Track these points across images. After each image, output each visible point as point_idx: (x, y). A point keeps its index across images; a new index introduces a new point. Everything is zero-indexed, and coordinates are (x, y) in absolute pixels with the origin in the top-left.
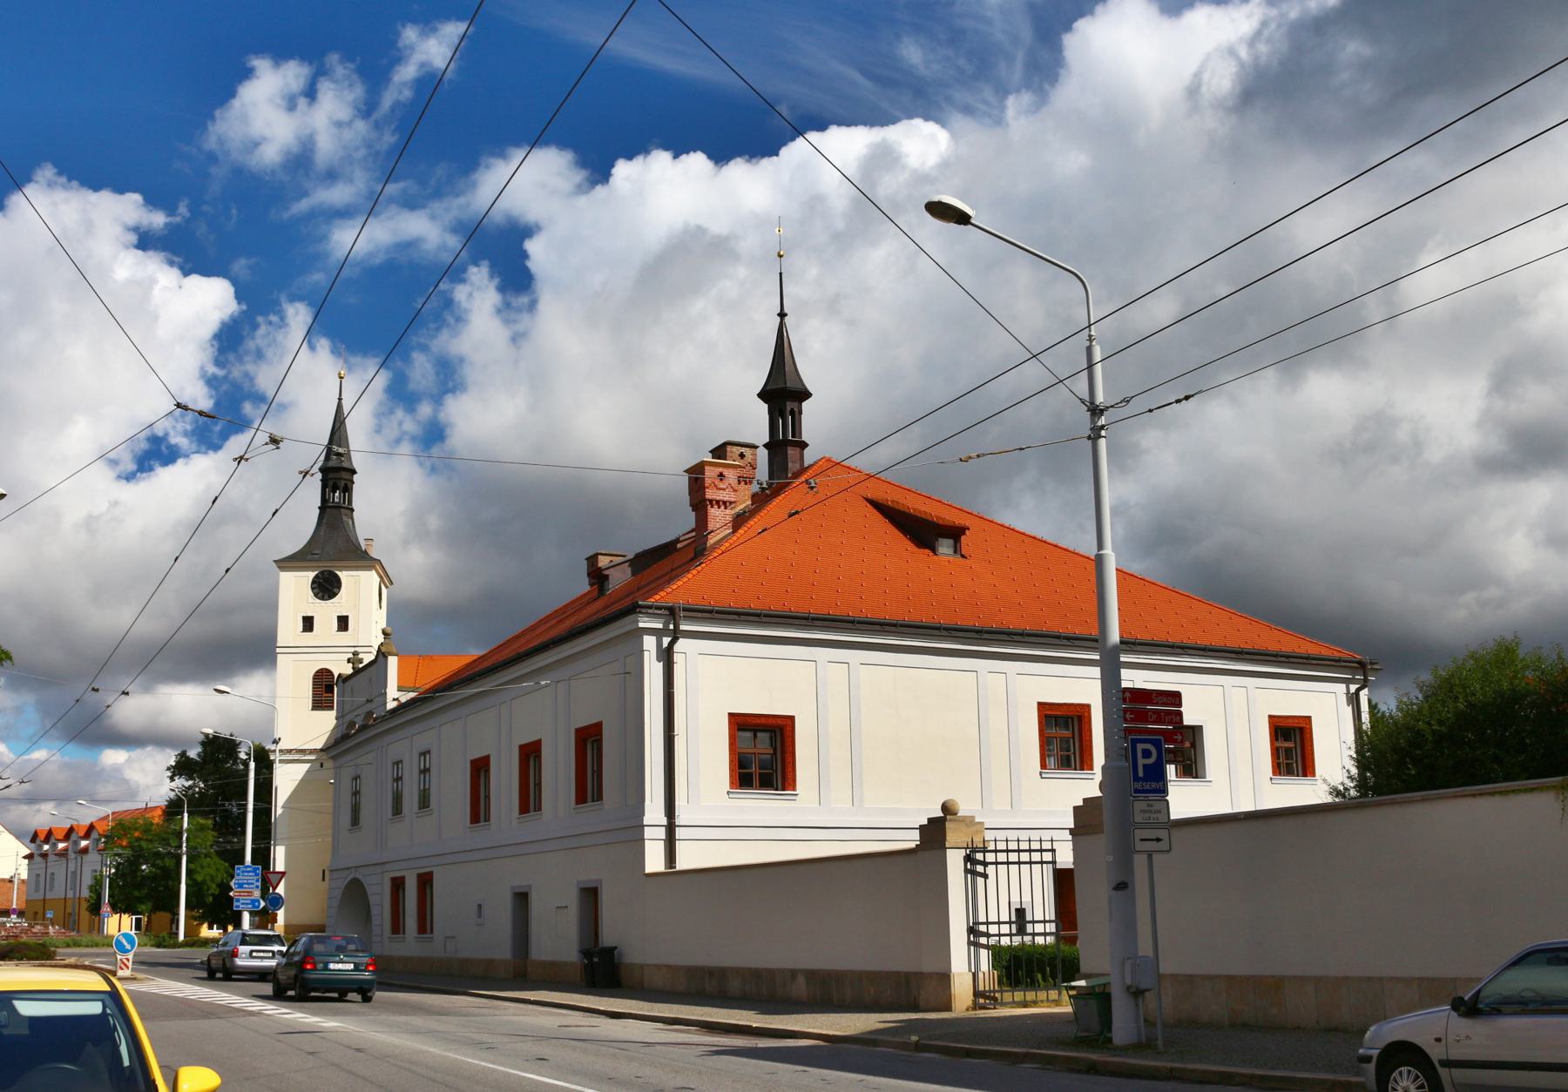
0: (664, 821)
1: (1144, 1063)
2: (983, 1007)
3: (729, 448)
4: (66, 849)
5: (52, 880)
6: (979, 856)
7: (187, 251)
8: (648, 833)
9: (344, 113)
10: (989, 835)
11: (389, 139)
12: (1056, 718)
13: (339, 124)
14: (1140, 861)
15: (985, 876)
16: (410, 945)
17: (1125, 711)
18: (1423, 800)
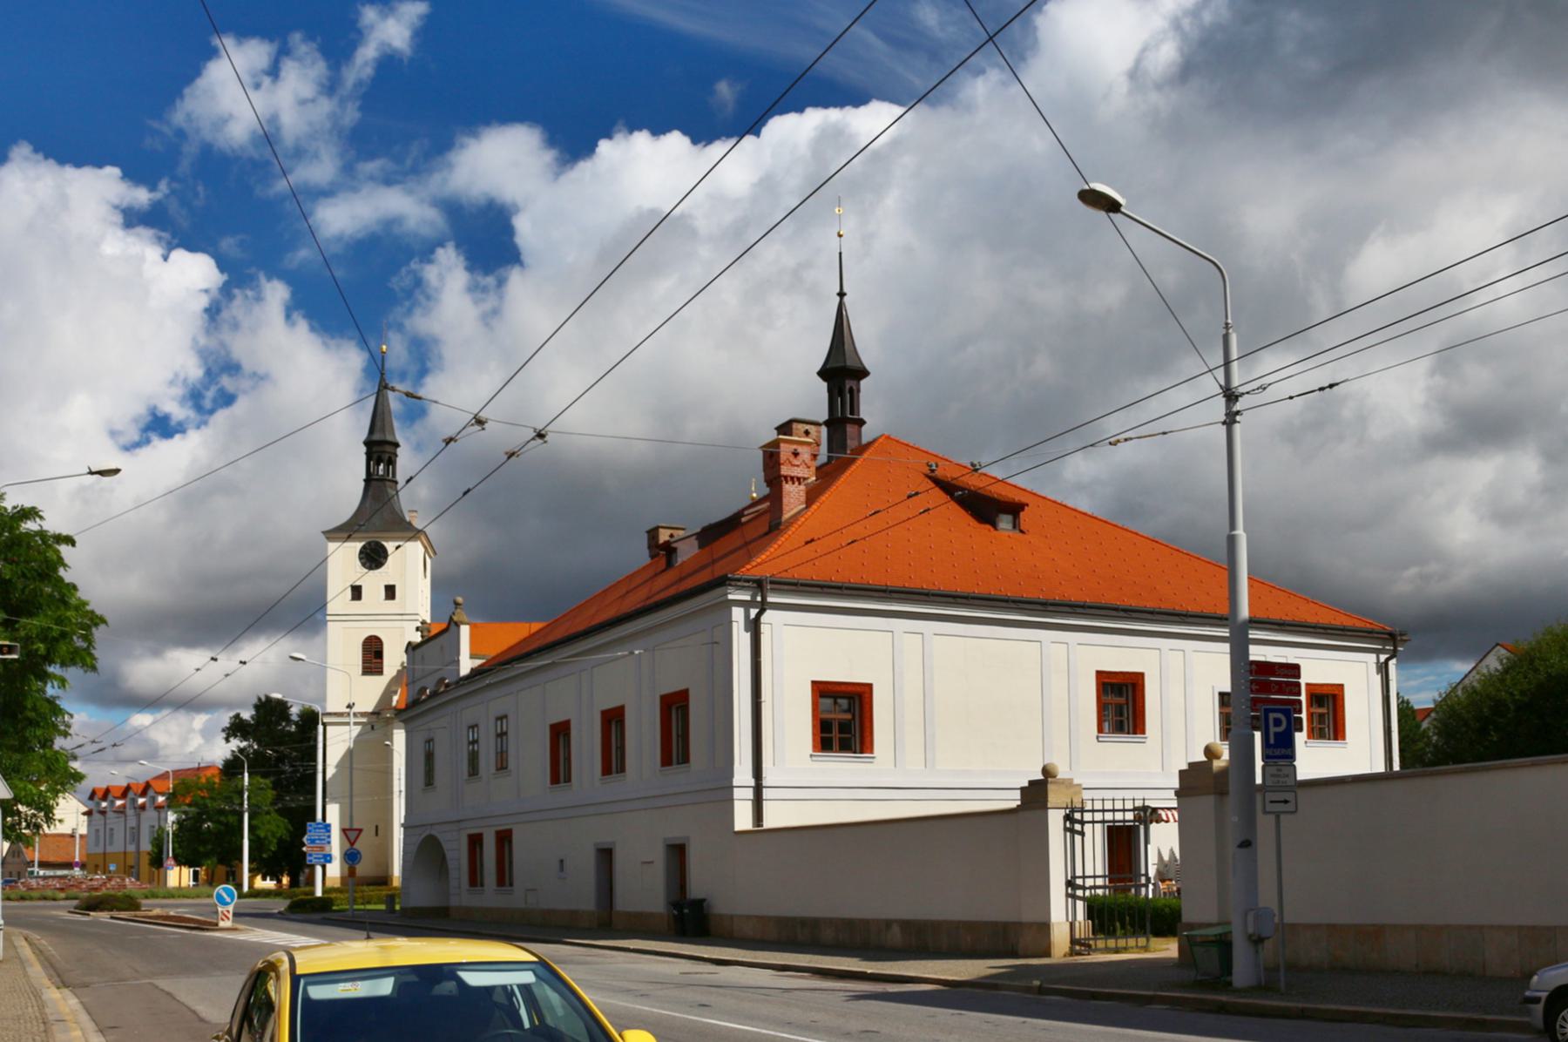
0: (752, 782)
1: (1275, 1003)
2: (1079, 954)
3: (795, 425)
4: (124, 806)
5: (112, 835)
6: (1077, 816)
7: (172, 226)
8: (737, 793)
9: (307, 90)
10: (1086, 795)
11: (351, 115)
12: (1112, 685)
13: (303, 102)
14: (1265, 824)
15: (1082, 834)
16: (490, 897)
17: (1252, 682)
18: (1533, 765)
